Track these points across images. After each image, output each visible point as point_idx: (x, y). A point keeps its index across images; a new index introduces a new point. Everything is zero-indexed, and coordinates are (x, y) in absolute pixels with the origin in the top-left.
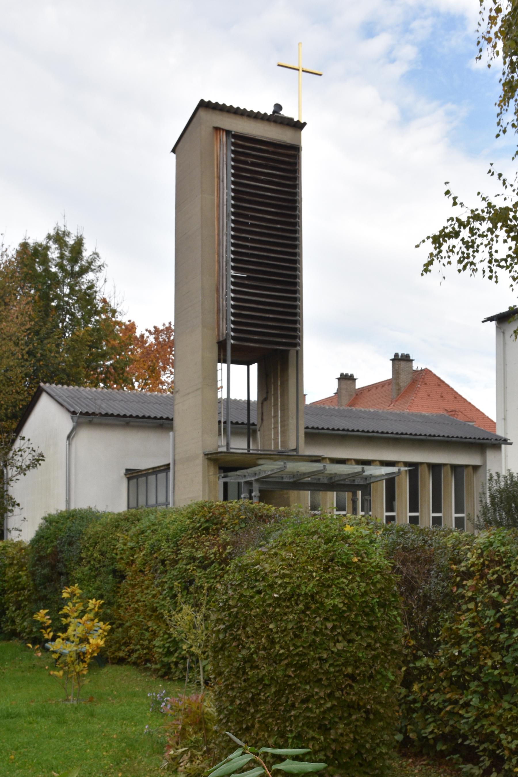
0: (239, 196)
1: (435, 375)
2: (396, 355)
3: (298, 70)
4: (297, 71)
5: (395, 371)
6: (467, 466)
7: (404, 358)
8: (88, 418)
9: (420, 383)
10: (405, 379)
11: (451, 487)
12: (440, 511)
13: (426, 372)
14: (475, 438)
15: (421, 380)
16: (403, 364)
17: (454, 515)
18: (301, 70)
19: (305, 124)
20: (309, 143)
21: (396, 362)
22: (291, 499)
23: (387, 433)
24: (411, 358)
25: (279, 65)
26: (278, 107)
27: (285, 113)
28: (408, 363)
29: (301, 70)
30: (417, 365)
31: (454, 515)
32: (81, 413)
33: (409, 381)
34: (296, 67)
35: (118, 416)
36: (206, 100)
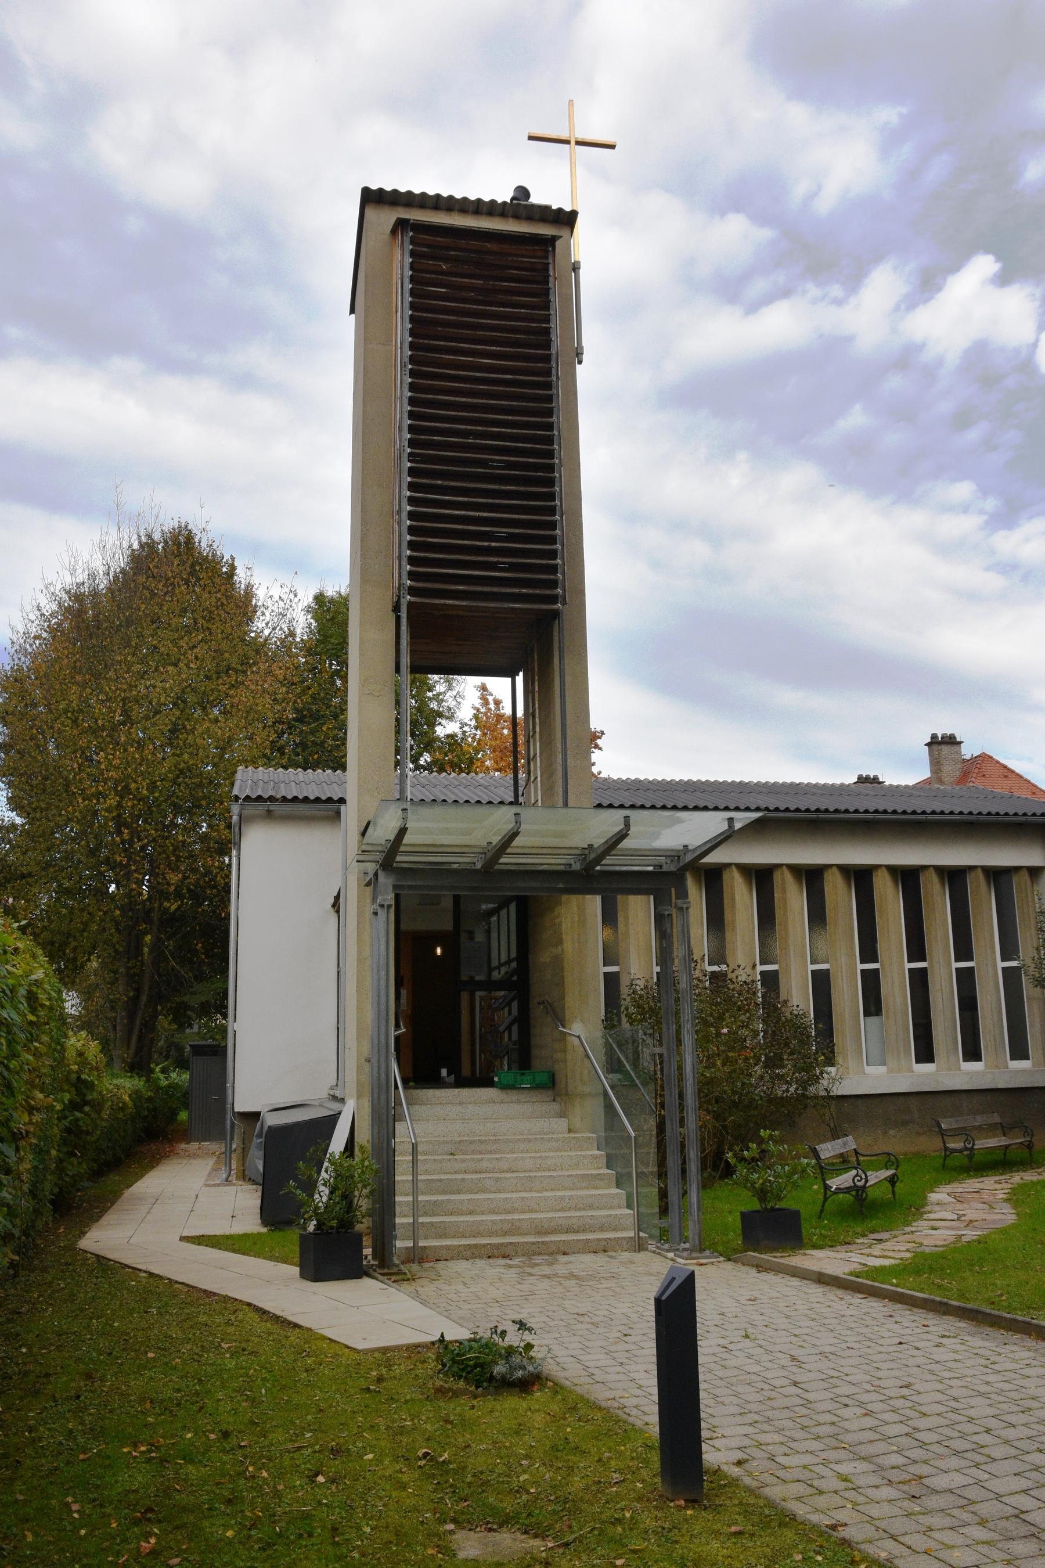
0: (419, 327)
1: (998, 762)
2: (934, 736)
3: (567, 142)
4: (567, 146)
5: (936, 764)
6: (1017, 869)
7: (946, 739)
8: (261, 808)
9: (974, 775)
10: (951, 771)
11: (991, 909)
12: (970, 958)
13: (984, 759)
14: (1025, 814)
15: (977, 770)
16: (945, 749)
17: (1001, 965)
18: (573, 142)
19: (574, 214)
20: (586, 245)
21: (935, 747)
22: (564, 926)
23: (847, 811)
24: (958, 739)
25: (531, 138)
26: (522, 193)
27: (535, 199)
28: (955, 748)
29: (573, 142)
30: (968, 751)
31: (1001, 965)
32: (248, 798)
33: (958, 773)
34: (564, 136)
35: (318, 800)
36: (374, 187)
